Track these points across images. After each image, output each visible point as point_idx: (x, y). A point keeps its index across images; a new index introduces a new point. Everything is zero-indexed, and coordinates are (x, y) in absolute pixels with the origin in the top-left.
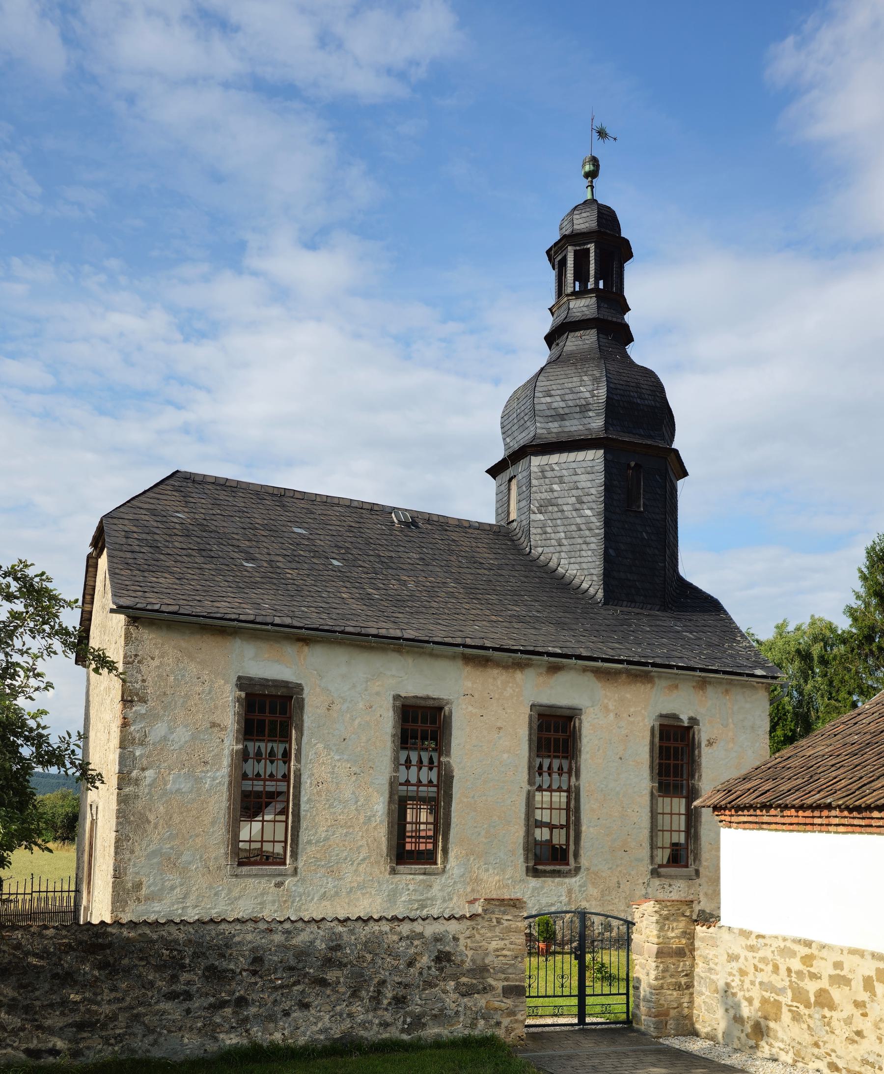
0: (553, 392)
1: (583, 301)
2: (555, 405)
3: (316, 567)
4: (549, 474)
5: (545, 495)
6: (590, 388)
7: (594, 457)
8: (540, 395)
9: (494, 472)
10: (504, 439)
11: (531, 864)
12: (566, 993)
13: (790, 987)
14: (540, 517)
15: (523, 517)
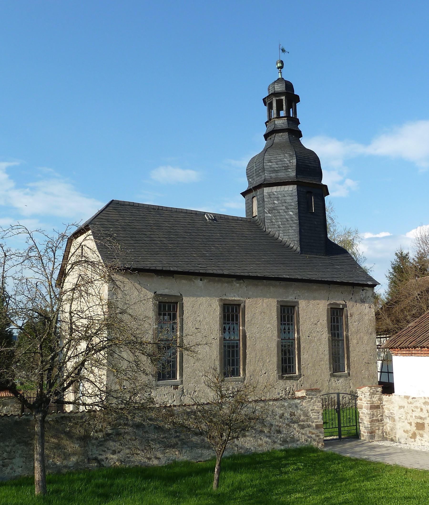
0: (272, 161)
2: (273, 166)
3: (180, 242)
4: (272, 196)
5: (270, 206)
6: (289, 159)
7: (292, 188)
8: (266, 162)
9: (244, 194)
10: (248, 179)
11: (280, 374)
15: (261, 215)
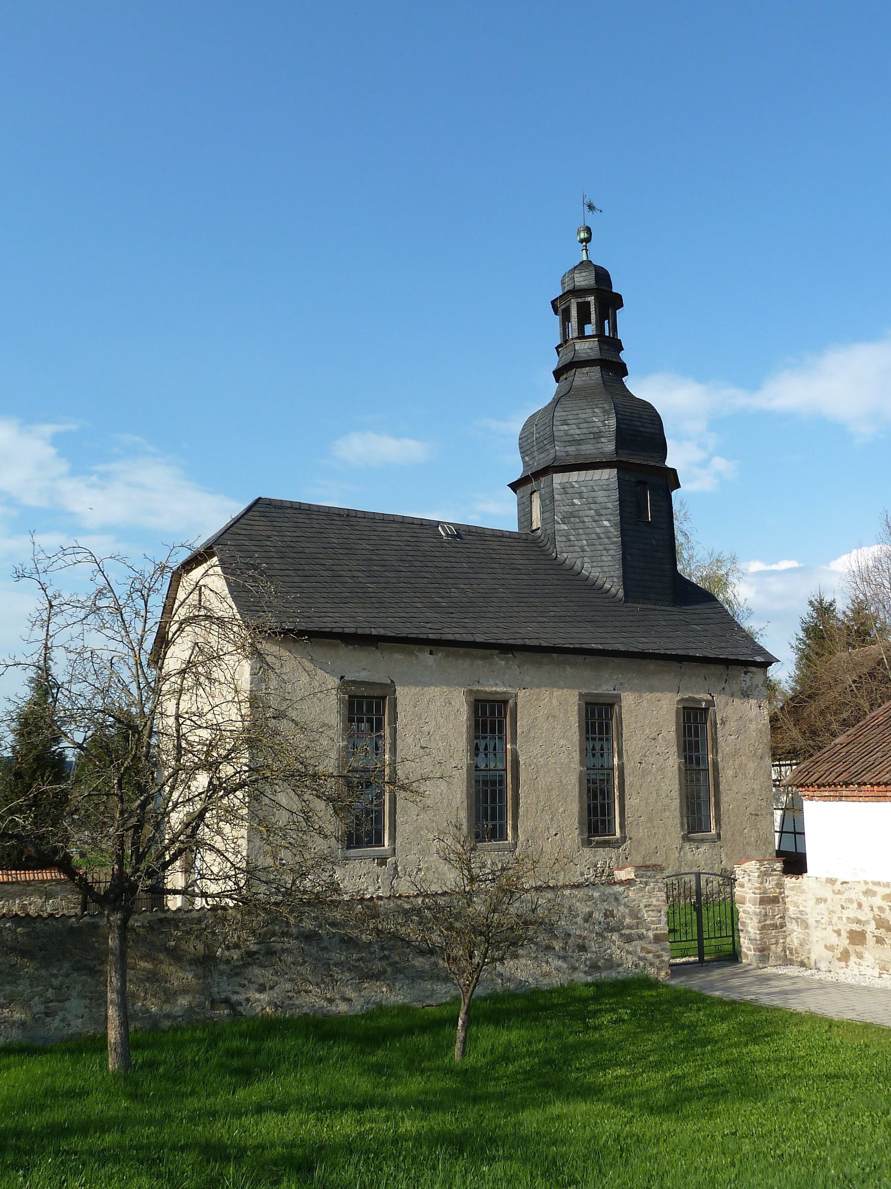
0: (569, 421)
1: (587, 344)
2: (572, 432)
4: (570, 490)
5: (567, 509)
6: (602, 418)
7: (608, 476)
8: (558, 423)
9: (514, 486)
10: (523, 458)
11: (586, 836)
12: (689, 938)
13: (874, 918)
14: (565, 527)
15: (548, 527)
